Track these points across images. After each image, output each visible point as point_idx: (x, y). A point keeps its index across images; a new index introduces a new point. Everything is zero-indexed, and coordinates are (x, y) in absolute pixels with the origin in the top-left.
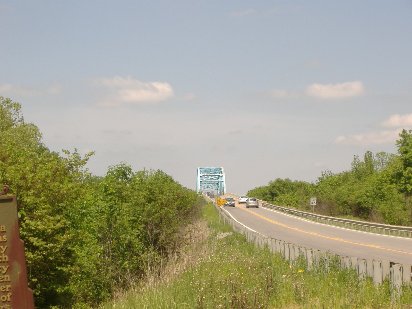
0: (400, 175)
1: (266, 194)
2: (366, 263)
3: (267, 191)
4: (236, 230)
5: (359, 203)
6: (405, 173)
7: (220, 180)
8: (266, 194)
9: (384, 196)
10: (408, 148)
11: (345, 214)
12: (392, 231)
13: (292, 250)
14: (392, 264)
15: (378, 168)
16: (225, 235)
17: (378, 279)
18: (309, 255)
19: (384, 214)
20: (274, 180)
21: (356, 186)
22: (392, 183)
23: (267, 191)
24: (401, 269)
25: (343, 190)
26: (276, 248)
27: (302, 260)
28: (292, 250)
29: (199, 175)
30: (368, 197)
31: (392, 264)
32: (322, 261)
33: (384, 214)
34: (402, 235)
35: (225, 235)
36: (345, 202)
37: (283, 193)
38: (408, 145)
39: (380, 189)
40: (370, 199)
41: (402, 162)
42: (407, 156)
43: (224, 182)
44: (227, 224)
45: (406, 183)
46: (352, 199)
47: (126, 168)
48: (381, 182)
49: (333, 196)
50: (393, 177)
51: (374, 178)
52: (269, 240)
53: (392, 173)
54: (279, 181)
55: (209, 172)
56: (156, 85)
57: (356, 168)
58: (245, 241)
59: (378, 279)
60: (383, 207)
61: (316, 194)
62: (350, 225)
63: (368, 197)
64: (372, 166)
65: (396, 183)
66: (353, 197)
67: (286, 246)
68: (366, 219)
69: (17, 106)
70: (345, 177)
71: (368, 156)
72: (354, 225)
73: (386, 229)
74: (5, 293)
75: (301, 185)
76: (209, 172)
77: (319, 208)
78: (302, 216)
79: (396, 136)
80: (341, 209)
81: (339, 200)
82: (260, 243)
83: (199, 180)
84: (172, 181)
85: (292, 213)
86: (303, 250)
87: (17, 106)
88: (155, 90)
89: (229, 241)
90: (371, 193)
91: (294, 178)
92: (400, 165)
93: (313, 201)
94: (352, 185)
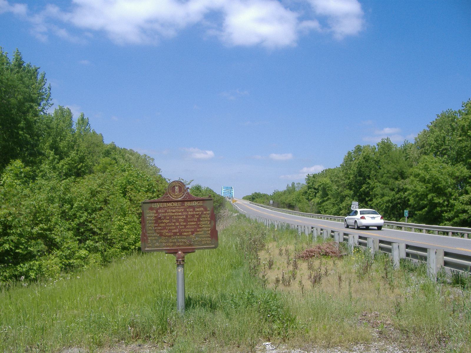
0: (306, 192)
1: (250, 198)
2: (301, 227)
3: (251, 197)
4: (241, 213)
5: (290, 203)
6: (308, 192)
7: (231, 192)
8: (250, 198)
9: (300, 201)
10: (310, 181)
11: (284, 207)
12: (304, 215)
13: (268, 221)
14: (312, 228)
15: (297, 189)
16: (236, 214)
17: (307, 233)
18: (276, 223)
19: (300, 208)
20: (254, 193)
21: (289, 196)
22: (303, 195)
23: (251, 197)
24: (317, 229)
25: (283, 198)
26: (260, 221)
27: (273, 226)
28: (268, 221)
29: (223, 189)
30: (293, 201)
31: (312, 228)
32: (282, 226)
33: (300, 208)
34: (308, 217)
35: (236, 214)
36: (284, 203)
37: (257, 198)
38: (310, 180)
39: (298, 198)
40: (295, 202)
41: (307, 187)
42: (309, 185)
43: (233, 193)
44: (236, 210)
45: (308, 196)
46: (287, 201)
47: (199, 186)
48: (299, 195)
49: (279, 200)
50: (303, 193)
51: (295, 193)
52: (257, 217)
53: (303, 191)
54: (256, 193)
55: (227, 188)
56: (207, 151)
57: (288, 189)
58: (245, 217)
59: (307, 233)
60: (300, 205)
61: (272, 199)
62: (287, 212)
63: (293, 201)
64: (294, 188)
65: (304, 195)
66: (287, 201)
67: (265, 219)
68: (293, 210)
69: (153, 159)
70: (285, 193)
71: (293, 184)
72: (388, 225)
73: (415, 228)
74: (209, 231)
75: (265, 195)
76: (227, 188)
77: (273, 205)
78: (266, 208)
79: (305, 176)
80: (282, 205)
81: (281, 202)
82: (253, 218)
83: (223, 192)
84: (213, 192)
85: (262, 207)
86: (273, 222)
87: (153, 159)
88: (206, 154)
89: (239, 217)
90: (295, 199)
91: (262, 192)
92: (306, 188)
93: (271, 202)
94: (287, 196)
